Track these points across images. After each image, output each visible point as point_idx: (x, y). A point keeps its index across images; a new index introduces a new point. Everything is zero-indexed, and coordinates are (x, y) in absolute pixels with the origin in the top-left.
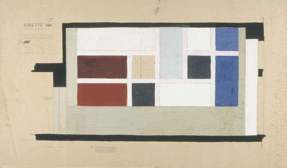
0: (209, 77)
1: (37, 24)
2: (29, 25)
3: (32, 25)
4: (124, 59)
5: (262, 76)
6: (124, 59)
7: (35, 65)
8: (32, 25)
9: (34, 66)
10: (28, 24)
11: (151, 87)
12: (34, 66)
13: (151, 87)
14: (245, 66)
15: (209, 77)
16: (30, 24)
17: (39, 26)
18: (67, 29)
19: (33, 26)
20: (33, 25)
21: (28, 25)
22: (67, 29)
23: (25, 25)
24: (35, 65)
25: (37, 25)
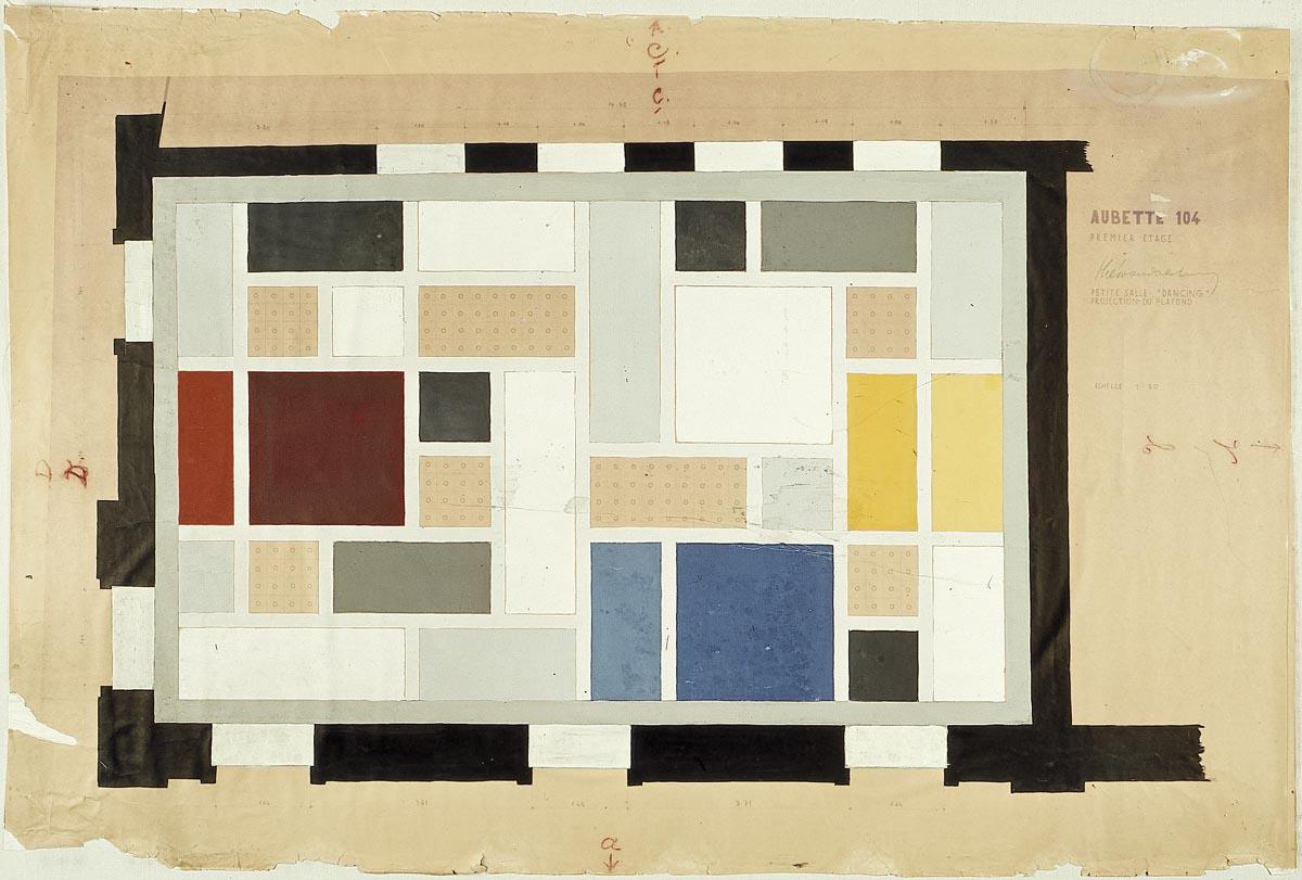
0: (855, 637)
1: (1142, 212)
2: (1110, 219)
3: (1121, 216)
4: (484, 436)
5: (629, 785)
6: (484, 436)
7: (113, 495)
8: (1121, 216)
9: (103, 506)
10: (1107, 212)
11: (906, 644)
12: (103, 506)
13: (906, 644)
14: (490, 579)
15: (855, 637)
16: (1113, 212)
17: (1150, 222)
18: (1015, 183)
19: (1125, 222)
20: (1125, 218)
21: (1107, 217)
22: (1015, 183)
23: (1095, 219)
24: (113, 495)
25: (1144, 217)
